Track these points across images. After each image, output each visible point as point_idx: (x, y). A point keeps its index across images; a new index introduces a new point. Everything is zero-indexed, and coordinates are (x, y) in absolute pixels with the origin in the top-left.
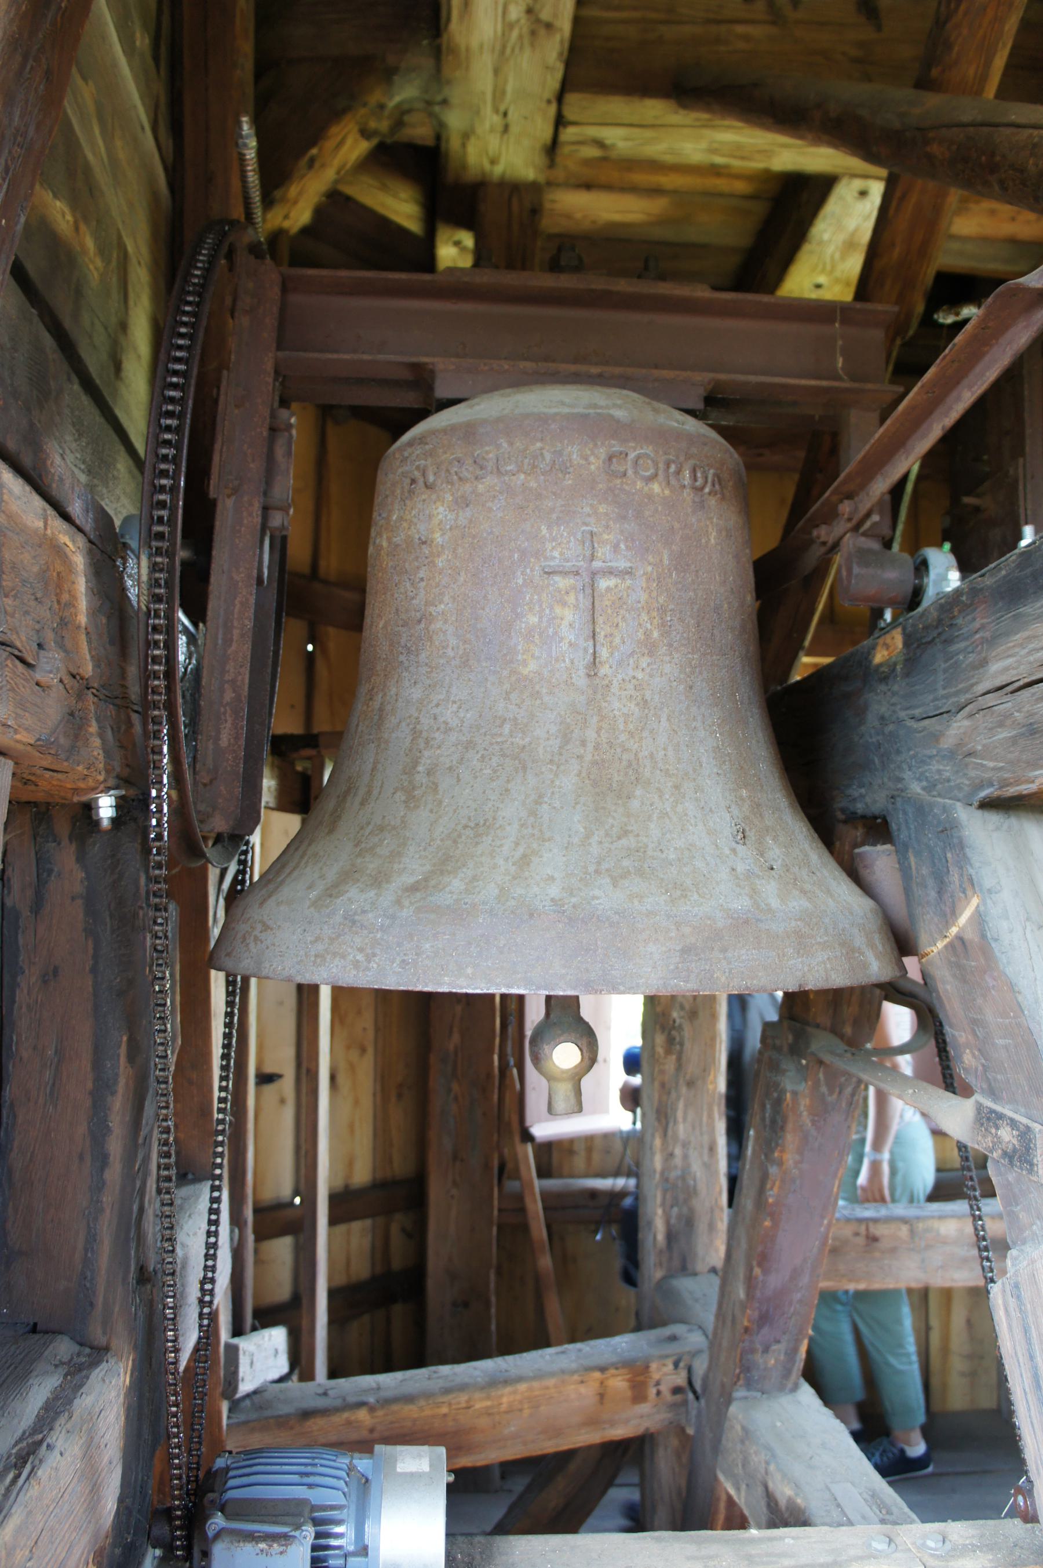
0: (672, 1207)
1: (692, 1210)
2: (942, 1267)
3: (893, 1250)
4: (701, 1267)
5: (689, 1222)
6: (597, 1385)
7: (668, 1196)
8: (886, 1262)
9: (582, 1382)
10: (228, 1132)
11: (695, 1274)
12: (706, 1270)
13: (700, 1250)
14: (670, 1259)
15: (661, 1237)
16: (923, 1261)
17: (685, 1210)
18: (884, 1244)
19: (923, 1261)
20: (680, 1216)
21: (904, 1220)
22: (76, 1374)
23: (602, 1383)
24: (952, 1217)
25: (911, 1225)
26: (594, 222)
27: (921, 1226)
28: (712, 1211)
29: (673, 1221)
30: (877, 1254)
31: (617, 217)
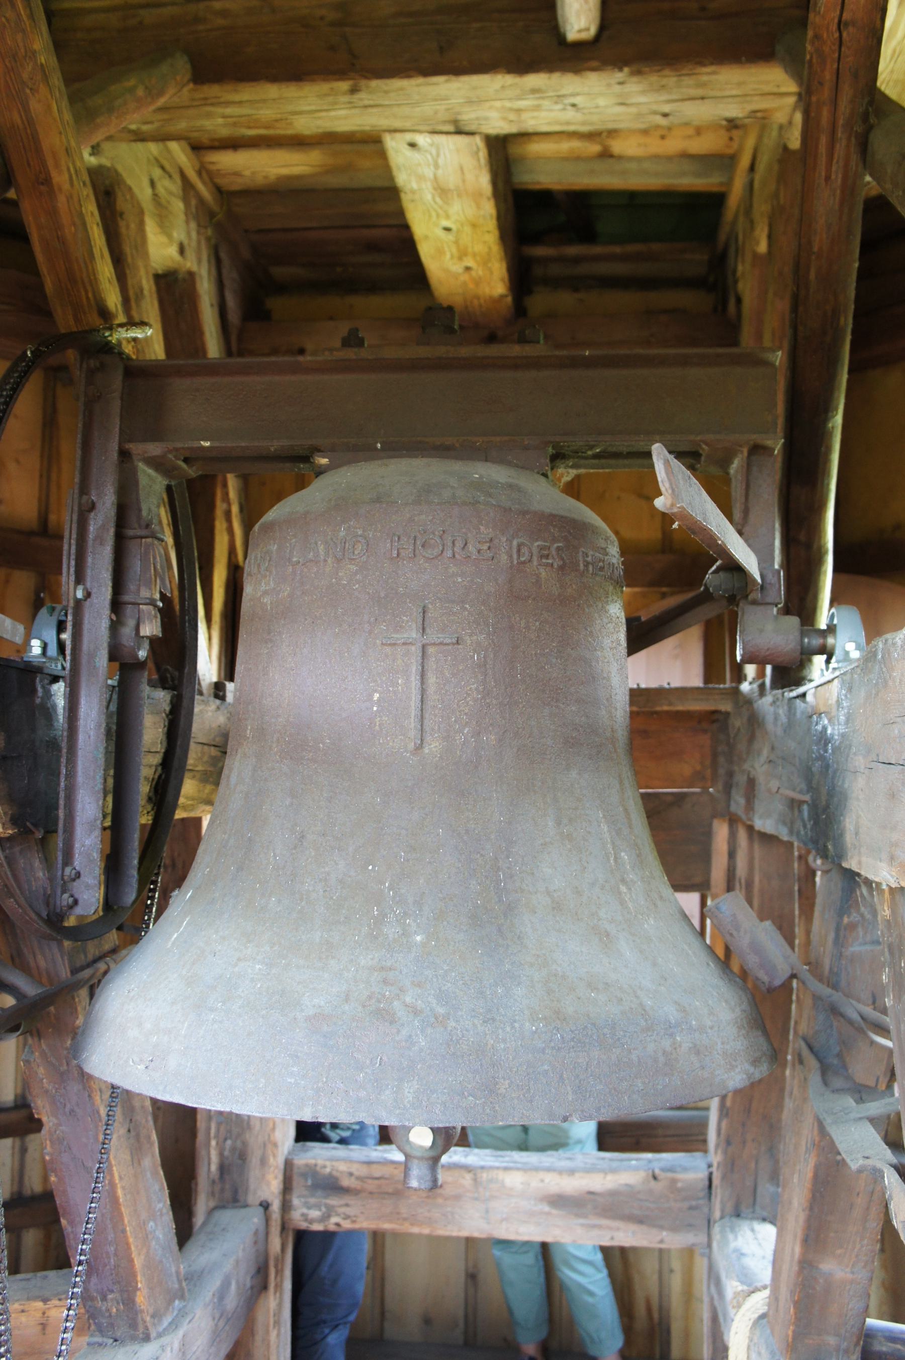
0: (225, 1139)
1: (245, 1144)
2: (505, 1220)
3: (457, 1197)
4: (253, 1199)
5: (242, 1156)
6: (39, 1314)
7: (222, 1128)
8: (449, 1209)
9: (23, 1311)
10: (147, 889)
11: (246, 1206)
12: (258, 1203)
13: (252, 1185)
14: (222, 1190)
15: (214, 1168)
16: (487, 1211)
17: (239, 1144)
18: (448, 1191)
19: (487, 1211)
20: (233, 1149)
21: (467, 1168)
22: (860, 889)
23: (44, 1313)
24: (518, 1169)
25: (475, 1174)
26: (266, 177)
27: (484, 1176)
28: (265, 1145)
29: (226, 1153)
30: (440, 1201)
31: (285, 171)
